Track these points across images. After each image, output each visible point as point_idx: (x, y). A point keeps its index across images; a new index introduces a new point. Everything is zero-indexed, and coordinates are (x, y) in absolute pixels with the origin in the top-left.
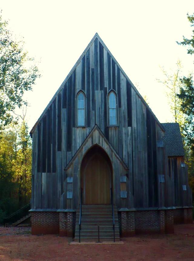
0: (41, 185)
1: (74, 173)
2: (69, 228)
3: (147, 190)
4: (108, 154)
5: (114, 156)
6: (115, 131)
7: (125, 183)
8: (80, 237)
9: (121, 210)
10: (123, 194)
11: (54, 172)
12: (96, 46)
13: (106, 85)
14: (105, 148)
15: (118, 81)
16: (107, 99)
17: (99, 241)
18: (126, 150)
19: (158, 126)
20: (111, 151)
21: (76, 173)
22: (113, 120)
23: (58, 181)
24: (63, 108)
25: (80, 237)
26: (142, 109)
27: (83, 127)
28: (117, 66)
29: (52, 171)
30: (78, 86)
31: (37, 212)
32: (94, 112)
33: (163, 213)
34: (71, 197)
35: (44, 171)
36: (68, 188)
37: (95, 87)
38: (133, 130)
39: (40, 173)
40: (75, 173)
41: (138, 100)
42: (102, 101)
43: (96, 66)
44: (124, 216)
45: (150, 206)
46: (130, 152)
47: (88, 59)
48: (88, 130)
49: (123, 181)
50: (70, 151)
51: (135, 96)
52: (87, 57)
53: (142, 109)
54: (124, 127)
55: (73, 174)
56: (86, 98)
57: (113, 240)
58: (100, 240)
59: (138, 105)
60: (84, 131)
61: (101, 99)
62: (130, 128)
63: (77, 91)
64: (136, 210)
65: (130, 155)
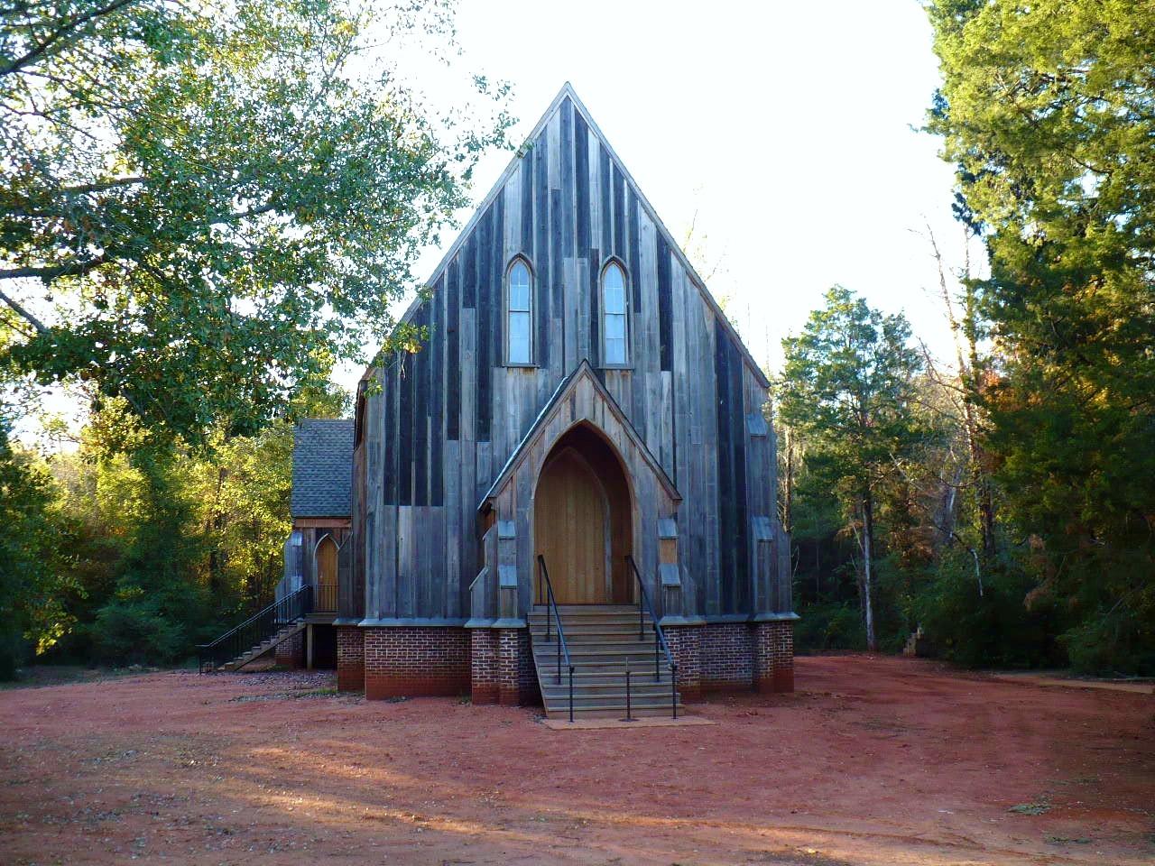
0: (397, 544)
1: (518, 507)
2: (507, 677)
3: (718, 563)
4: (620, 451)
5: (638, 459)
6: (623, 380)
7: (672, 539)
8: (571, 706)
9: (666, 620)
10: (670, 576)
11: (437, 505)
12: (564, 121)
13: (596, 242)
14: (613, 432)
15: (631, 232)
16: (599, 286)
17: (629, 717)
18: (658, 438)
19: (749, 371)
20: (628, 442)
21: (523, 510)
22: (615, 352)
23: (449, 533)
24: (465, 305)
25: (571, 706)
26: (702, 319)
27: (528, 369)
28: (629, 185)
29: (429, 503)
30: (509, 240)
31: (383, 628)
32: (558, 322)
33: (764, 630)
34: (513, 582)
35: (406, 502)
36: (500, 555)
37: (563, 247)
38: (675, 377)
39: (393, 507)
40: (519, 510)
41: (692, 293)
42: (583, 289)
43: (567, 181)
44: (670, 639)
45: (726, 609)
46: (668, 449)
47: (541, 159)
48: (539, 378)
49: (668, 535)
50: (487, 440)
51: (681, 281)
52: (538, 153)
53: (702, 319)
54: (651, 369)
55: (514, 510)
56: (536, 280)
57: (671, 712)
58: (632, 713)
59: (690, 307)
60: (528, 379)
61: (582, 284)
62: (666, 375)
63: (508, 256)
64: (705, 622)
65: (667, 455)
